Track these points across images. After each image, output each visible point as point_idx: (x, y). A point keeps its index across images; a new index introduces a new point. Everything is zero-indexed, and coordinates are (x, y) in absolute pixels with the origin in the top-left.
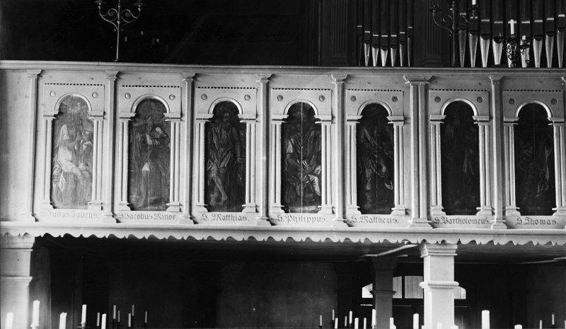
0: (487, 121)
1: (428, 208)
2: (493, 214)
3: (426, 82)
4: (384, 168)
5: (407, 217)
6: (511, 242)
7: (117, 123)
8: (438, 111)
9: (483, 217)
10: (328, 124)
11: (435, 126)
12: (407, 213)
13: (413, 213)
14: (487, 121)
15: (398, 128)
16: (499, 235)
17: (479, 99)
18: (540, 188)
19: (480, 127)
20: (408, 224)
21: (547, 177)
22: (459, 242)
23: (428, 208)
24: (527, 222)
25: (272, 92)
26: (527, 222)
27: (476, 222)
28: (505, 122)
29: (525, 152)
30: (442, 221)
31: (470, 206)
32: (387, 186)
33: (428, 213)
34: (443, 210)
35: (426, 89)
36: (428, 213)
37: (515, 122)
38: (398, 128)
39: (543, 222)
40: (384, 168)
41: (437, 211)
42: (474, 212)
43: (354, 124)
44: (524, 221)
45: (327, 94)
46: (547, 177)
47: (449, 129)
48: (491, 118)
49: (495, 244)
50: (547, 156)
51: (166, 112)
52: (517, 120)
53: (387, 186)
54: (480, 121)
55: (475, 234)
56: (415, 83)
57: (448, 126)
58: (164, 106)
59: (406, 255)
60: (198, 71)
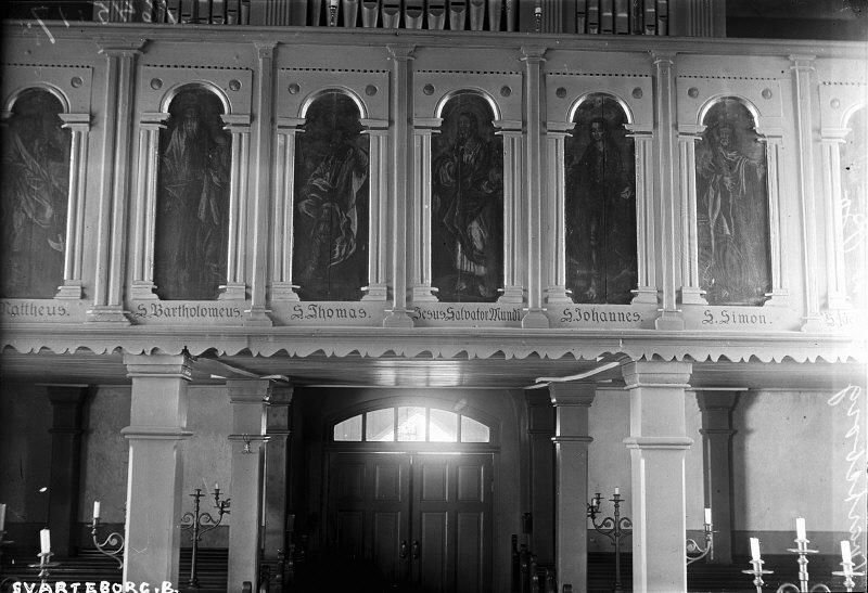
0: (247, 125)
1: (125, 287)
2: (248, 297)
3: (135, 51)
4: (49, 212)
5: (84, 302)
6: (356, 352)
7: (136, 130)
8: (157, 106)
9: (230, 305)
10: (517, 136)
11: (149, 133)
12: (83, 296)
13: (97, 299)
14: (247, 125)
15: (79, 134)
16: (262, 336)
17: (371, 90)
18: (341, 249)
19: (235, 138)
20: (86, 314)
21: (355, 229)
22: (185, 352)
23: (125, 287)
24: (312, 312)
25: (142, 69)
26: (312, 312)
27: (215, 312)
28: (416, 127)
29: (315, 183)
30: (576, 315)
31: (487, 286)
32: (53, 244)
33: (124, 296)
34: (154, 291)
35: (135, 61)
36: (124, 296)
37: (299, 127)
38: (79, 134)
39: (341, 313)
40: (49, 212)
41: (143, 291)
42: (212, 294)
43: (154, 129)
44: (307, 312)
45: (85, 76)
46: (355, 229)
47: (178, 141)
48: (391, 122)
49: (508, 357)
50: (355, 188)
51: (223, 112)
52: (303, 122)
53: (53, 244)
54: (372, 128)
55: (216, 335)
56: (114, 51)
57: (175, 133)
58: (59, 102)
59: (213, 376)
60: (283, 38)
